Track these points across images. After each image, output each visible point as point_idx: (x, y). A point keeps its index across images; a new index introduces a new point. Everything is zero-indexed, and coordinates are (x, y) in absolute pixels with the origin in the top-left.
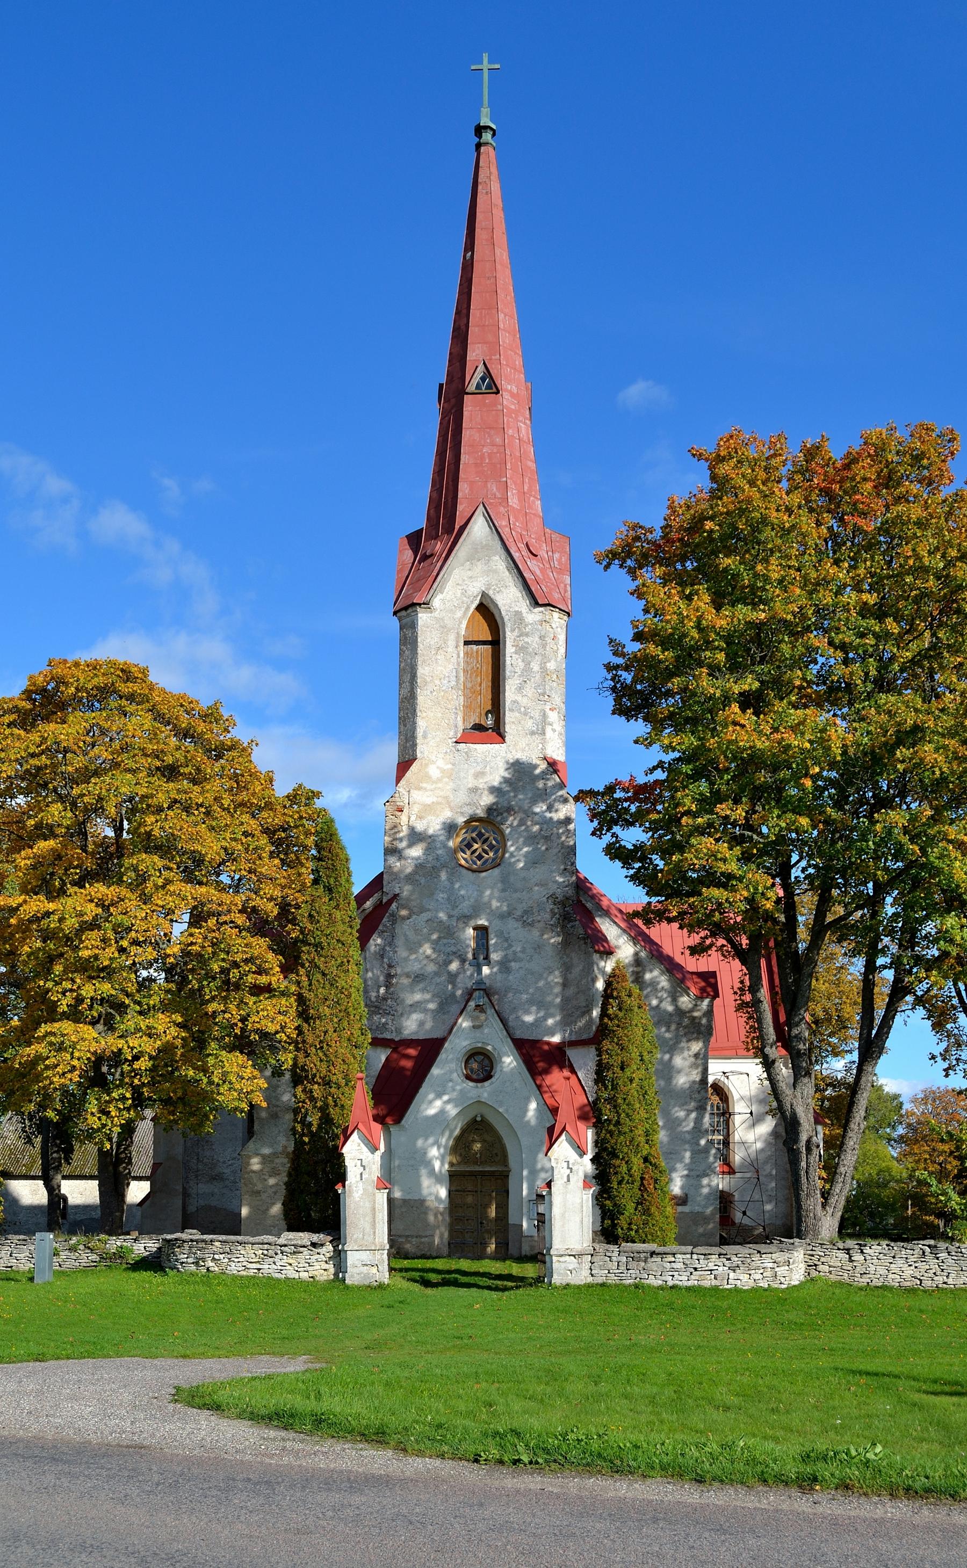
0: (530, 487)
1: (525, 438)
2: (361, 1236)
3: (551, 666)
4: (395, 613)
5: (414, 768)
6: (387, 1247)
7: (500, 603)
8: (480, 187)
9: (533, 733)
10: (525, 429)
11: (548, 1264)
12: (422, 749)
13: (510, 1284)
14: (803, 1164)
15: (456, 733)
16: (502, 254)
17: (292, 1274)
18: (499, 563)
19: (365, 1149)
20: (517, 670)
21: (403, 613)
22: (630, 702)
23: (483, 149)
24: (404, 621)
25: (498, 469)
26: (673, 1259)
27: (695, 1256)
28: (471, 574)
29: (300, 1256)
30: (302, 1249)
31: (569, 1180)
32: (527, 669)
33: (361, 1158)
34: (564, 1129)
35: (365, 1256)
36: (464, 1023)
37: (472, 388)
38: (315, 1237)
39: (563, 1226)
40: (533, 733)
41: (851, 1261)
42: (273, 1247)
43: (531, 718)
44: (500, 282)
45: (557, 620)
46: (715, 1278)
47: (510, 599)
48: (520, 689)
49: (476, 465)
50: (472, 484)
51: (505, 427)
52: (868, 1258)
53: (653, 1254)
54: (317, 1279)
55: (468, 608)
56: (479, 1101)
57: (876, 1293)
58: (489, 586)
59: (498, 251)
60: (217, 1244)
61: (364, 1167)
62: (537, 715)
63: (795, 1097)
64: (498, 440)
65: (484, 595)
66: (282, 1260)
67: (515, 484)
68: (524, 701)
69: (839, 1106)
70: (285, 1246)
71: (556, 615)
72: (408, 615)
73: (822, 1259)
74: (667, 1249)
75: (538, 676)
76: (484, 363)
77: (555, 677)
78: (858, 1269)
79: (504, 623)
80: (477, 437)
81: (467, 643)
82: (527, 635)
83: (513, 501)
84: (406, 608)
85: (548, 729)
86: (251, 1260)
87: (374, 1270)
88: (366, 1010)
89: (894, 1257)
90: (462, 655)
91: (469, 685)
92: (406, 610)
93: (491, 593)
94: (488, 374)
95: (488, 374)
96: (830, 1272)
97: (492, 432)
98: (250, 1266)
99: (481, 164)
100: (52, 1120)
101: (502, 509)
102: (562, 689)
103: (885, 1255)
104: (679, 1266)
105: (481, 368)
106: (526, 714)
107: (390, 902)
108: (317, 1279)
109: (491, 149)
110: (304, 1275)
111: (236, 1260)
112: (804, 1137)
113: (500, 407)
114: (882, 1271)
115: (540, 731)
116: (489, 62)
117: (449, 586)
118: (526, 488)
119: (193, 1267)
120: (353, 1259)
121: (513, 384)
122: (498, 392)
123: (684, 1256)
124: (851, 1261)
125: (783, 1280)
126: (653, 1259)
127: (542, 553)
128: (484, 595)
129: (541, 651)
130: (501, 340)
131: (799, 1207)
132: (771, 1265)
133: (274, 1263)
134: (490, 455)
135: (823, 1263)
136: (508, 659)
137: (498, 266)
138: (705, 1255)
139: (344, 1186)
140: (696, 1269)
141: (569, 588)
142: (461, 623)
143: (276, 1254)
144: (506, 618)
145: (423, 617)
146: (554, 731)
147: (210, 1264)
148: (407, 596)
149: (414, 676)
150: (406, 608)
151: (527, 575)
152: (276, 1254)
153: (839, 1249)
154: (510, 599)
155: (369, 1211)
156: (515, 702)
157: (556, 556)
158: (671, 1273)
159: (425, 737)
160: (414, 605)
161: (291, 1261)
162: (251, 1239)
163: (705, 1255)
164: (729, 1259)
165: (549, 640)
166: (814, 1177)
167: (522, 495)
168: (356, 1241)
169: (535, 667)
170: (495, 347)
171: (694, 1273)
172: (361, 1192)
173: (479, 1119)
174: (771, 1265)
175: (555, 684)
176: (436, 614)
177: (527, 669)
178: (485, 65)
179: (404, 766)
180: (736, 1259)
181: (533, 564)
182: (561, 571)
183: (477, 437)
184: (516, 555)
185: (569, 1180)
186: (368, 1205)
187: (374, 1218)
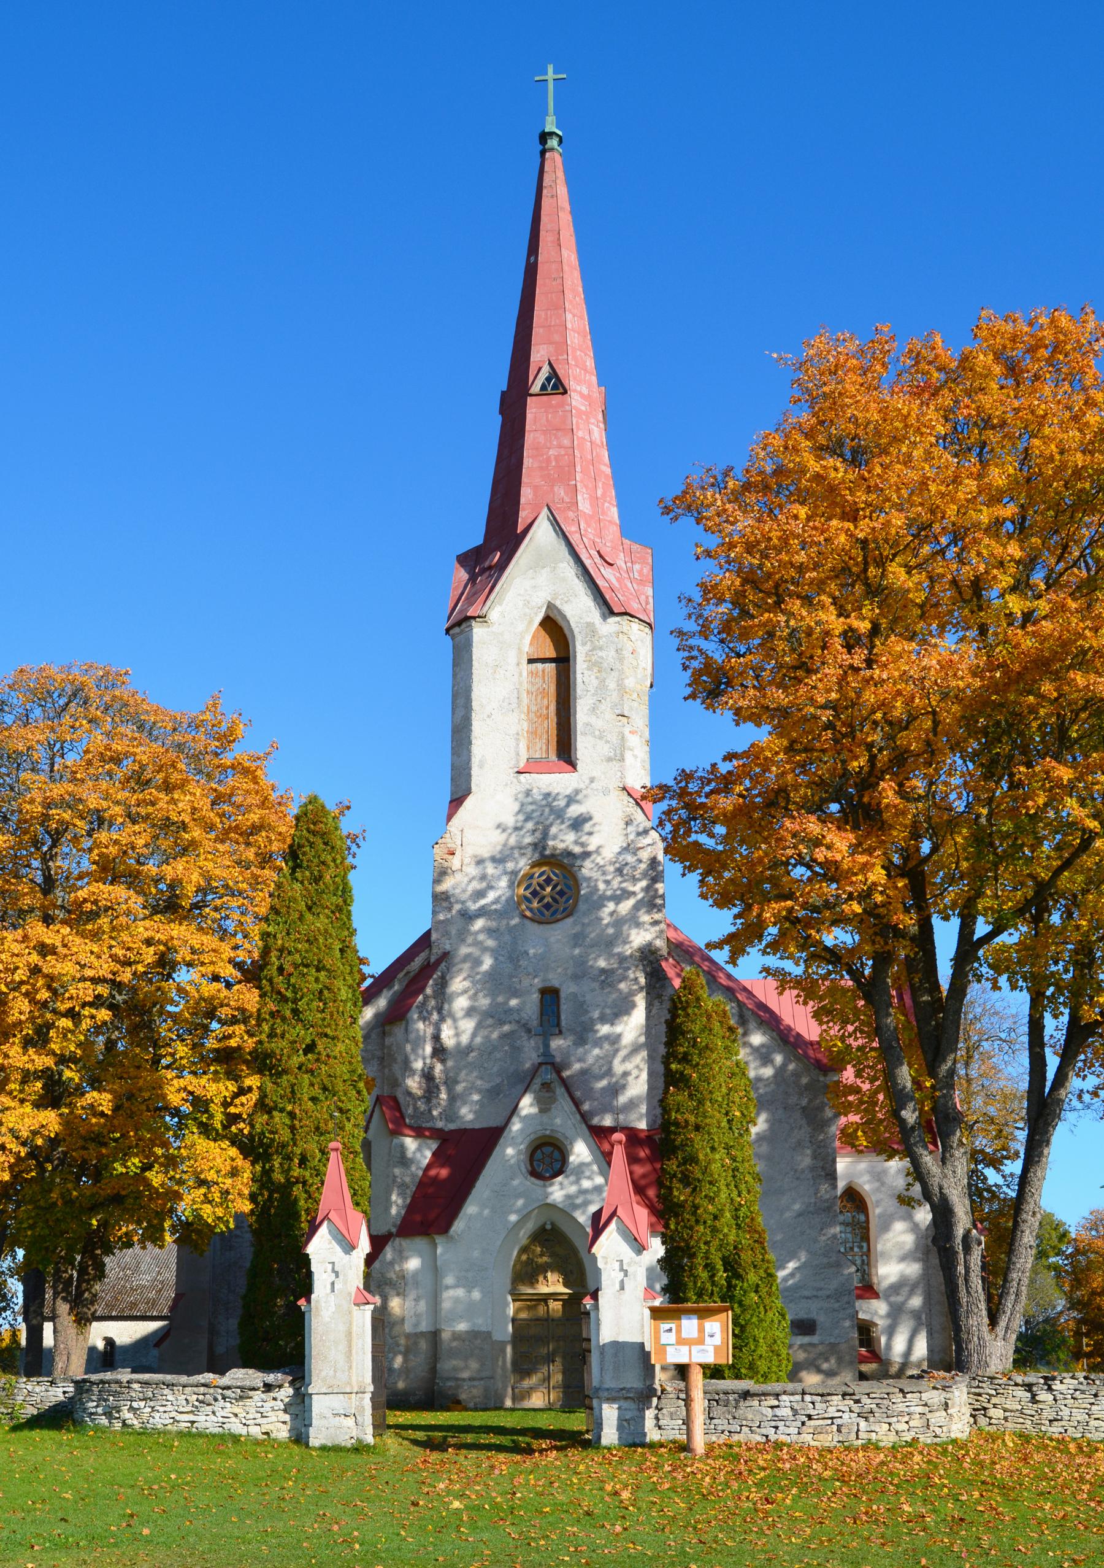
0: (604, 494)
1: (598, 442)
2: (332, 1373)
3: (630, 682)
4: (448, 631)
5: (468, 803)
6: (371, 1388)
8: (545, 192)
9: (609, 760)
10: (598, 433)
11: (596, 1411)
12: (479, 778)
14: (961, 1269)
15: (518, 761)
16: (570, 256)
17: (236, 1427)
18: (568, 569)
19: (338, 1249)
20: (591, 688)
21: (456, 630)
22: (711, 685)
23: (548, 155)
24: (457, 639)
25: (565, 473)
26: (776, 1403)
27: (808, 1398)
28: (536, 579)
29: (248, 1402)
30: (251, 1393)
31: (622, 1288)
33: (335, 1261)
34: (614, 1214)
35: (337, 1402)
36: (527, 1105)
37: (536, 388)
38: (271, 1378)
40: (609, 760)
41: (1034, 1400)
42: (211, 1391)
43: (607, 742)
44: (568, 283)
45: (636, 629)
46: (839, 1431)
47: (579, 609)
48: (593, 709)
49: (541, 468)
50: (536, 489)
51: (575, 432)
52: (1059, 1396)
53: (746, 1395)
55: (531, 622)
59: (565, 253)
60: (136, 1386)
61: (337, 1274)
62: (614, 739)
63: (945, 1176)
64: (566, 442)
65: (550, 606)
66: (224, 1409)
67: (586, 487)
68: (598, 723)
69: (1003, 1220)
70: (228, 1388)
71: (636, 626)
72: (462, 632)
73: (994, 1400)
74: (768, 1387)
75: (615, 694)
76: (550, 364)
77: (635, 696)
78: (1045, 1414)
80: (541, 439)
81: (531, 661)
82: (601, 649)
83: (584, 505)
84: (459, 624)
85: (628, 755)
86: (181, 1409)
87: (350, 1422)
89: (1096, 1395)
90: (525, 674)
91: (534, 708)
92: (460, 625)
93: (558, 603)
94: (554, 374)
95: (554, 374)
96: (1006, 1419)
97: (560, 433)
99: (546, 168)
101: (571, 514)
102: (644, 710)
103: (1083, 1392)
104: (785, 1412)
105: (546, 369)
106: (601, 738)
107: (439, 962)
108: (273, 1436)
109: (557, 156)
110: (255, 1431)
111: (162, 1409)
112: (960, 1232)
113: (568, 408)
114: (1082, 1417)
115: (618, 757)
116: (555, 73)
118: (599, 492)
119: (104, 1421)
120: (320, 1405)
121: (584, 386)
122: (565, 392)
123: (792, 1398)
124: (1034, 1400)
125: (938, 1431)
126: (747, 1403)
127: (620, 563)
128: (550, 606)
129: (618, 666)
130: (569, 335)
131: (958, 1329)
132: (920, 1409)
133: (214, 1413)
134: (557, 458)
135: (995, 1406)
136: (579, 676)
137: (565, 268)
138: (822, 1395)
139: (309, 1301)
140: (810, 1417)
141: (651, 600)
142: (523, 638)
143: (216, 1400)
144: (576, 631)
145: (478, 632)
146: (636, 757)
147: (127, 1415)
148: (461, 611)
149: (468, 700)
150: (459, 624)
151: (600, 582)
152: (216, 1400)
153: (1016, 1385)
154: (579, 609)
157: (637, 567)
158: (773, 1424)
159: (481, 766)
160: (468, 619)
161: (236, 1410)
162: (184, 1379)
163: (822, 1395)
164: (857, 1401)
165: (626, 653)
166: (978, 1320)
167: (594, 500)
168: (324, 1380)
169: (612, 685)
170: (562, 346)
171: (808, 1423)
172: (333, 1309)
173: (548, 1227)
174: (920, 1409)
175: (635, 704)
176: (494, 628)
178: (550, 75)
179: (457, 802)
180: (869, 1401)
181: (607, 572)
182: (641, 582)
183: (541, 439)
184: (588, 562)
185: (622, 1288)
186: (342, 1328)
187: (350, 1346)
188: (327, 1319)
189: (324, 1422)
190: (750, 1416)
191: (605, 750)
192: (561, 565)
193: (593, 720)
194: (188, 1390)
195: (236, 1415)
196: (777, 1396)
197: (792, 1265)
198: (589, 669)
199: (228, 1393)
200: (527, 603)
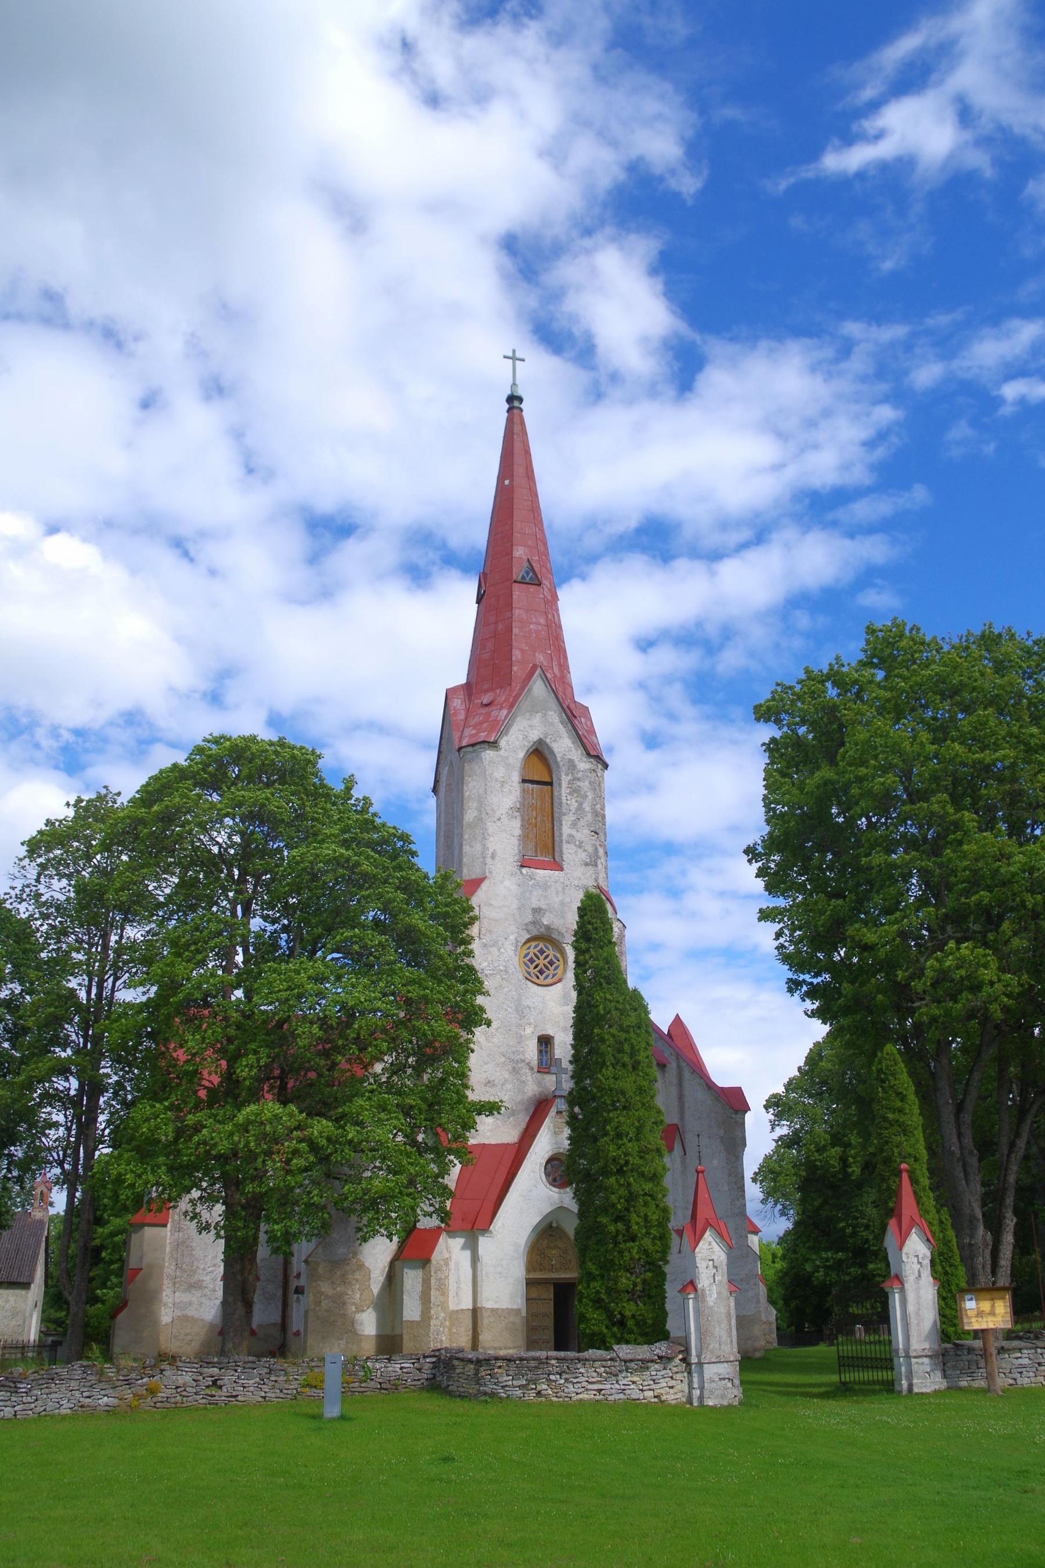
7: (556, 750)
13: (877, 1387)
18: (555, 716)
26: (1019, 1355)
30: (650, 1364)
32: (580, 808)
39: (918, 1325)
40: (586, 864)
43: (585, 851)
48: (574, 825)
50: (522, 651)
54: (663, 1398)
56: (561, 1207)
57: (483, 1398)
58: (546, 735)
75: (589, 815)
79: (558, 766)
81: (524, 781)
82: (579, 779)
88: (292, 1107)
98: (590, 1387)
100: (1016, 1224)
106: (580, 847)
117: (514, 730)
126: (1001, 1356)
154: (564, 746)
155: (724, 1316)
156: (570, 835)
159: (493, 857)
161: (635, 1379)
168: (712, 1352)
169: (587, 807)
176: (502, 752)
177: (580, 808)
183: (524, 615)
188: (712, 1304)
189: (714, 1385)
190: (1004, 1366)
191: (583, 856)
192: (550, 713)
193: (573, 832)
194: (597, 1364)
195: (634, 1382)
196: (1020, 1349)
197: (914, 1254)
198: (570, 794)
199: (633, 1364)
200: (526, 737)
